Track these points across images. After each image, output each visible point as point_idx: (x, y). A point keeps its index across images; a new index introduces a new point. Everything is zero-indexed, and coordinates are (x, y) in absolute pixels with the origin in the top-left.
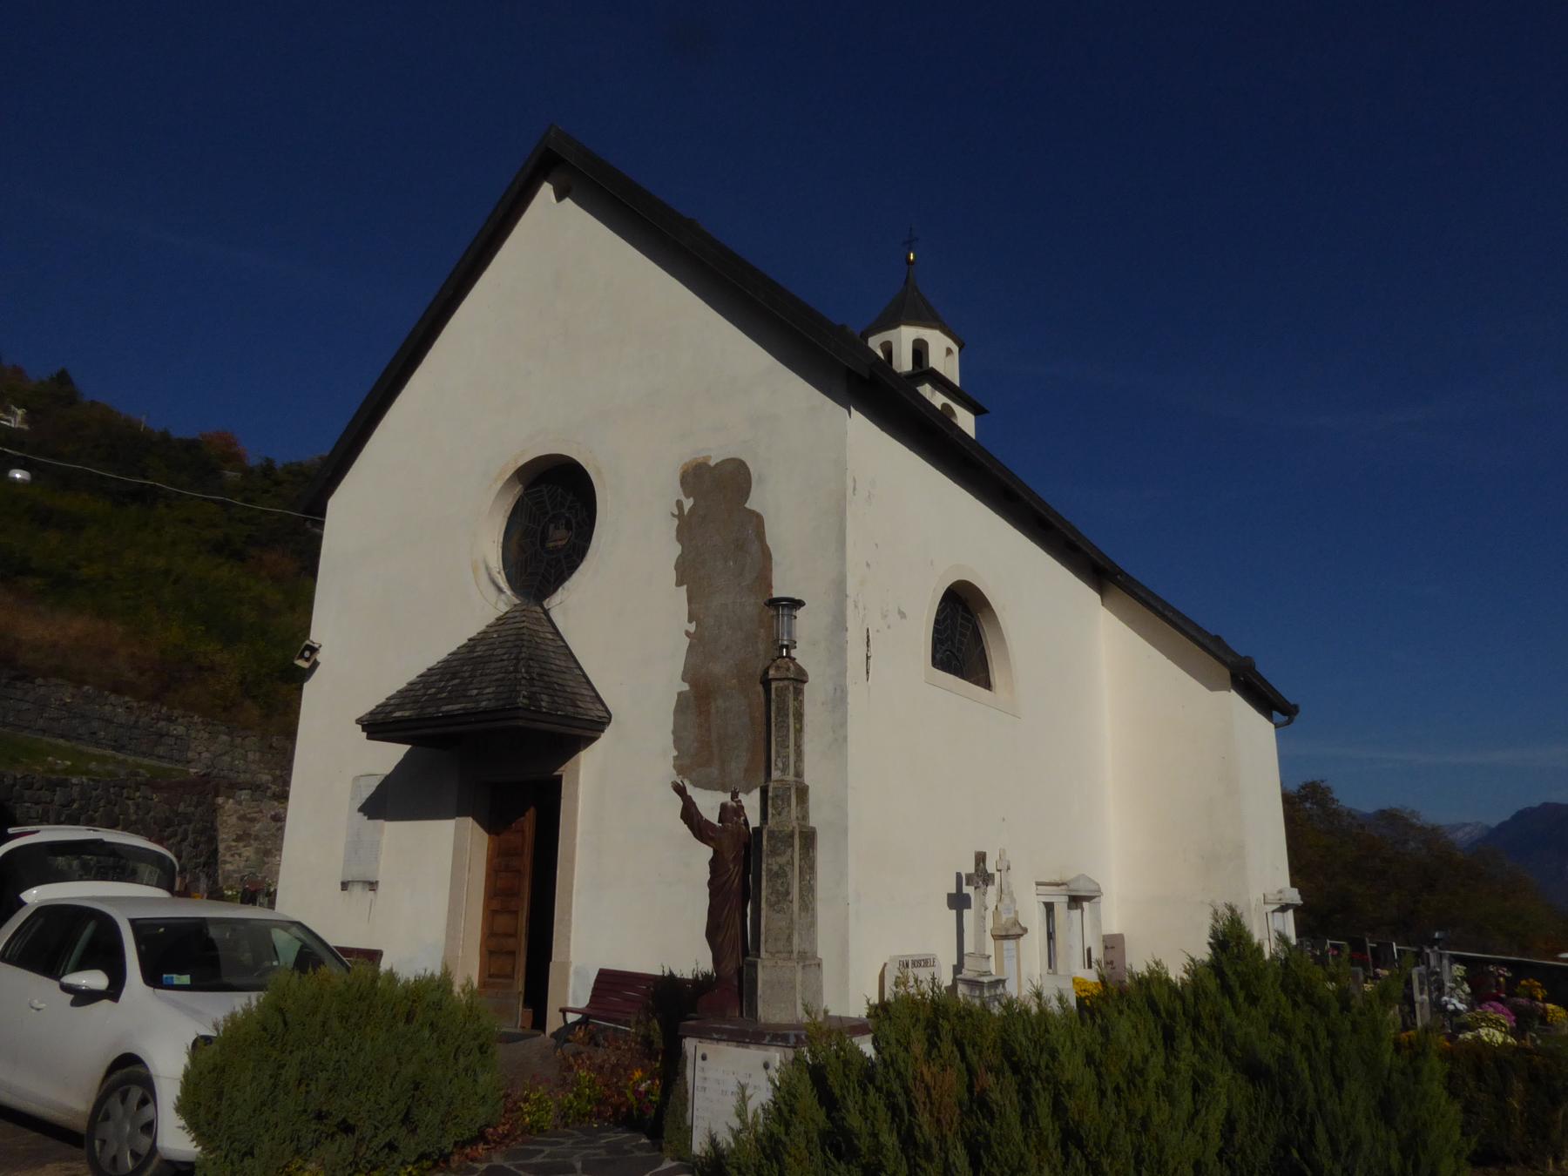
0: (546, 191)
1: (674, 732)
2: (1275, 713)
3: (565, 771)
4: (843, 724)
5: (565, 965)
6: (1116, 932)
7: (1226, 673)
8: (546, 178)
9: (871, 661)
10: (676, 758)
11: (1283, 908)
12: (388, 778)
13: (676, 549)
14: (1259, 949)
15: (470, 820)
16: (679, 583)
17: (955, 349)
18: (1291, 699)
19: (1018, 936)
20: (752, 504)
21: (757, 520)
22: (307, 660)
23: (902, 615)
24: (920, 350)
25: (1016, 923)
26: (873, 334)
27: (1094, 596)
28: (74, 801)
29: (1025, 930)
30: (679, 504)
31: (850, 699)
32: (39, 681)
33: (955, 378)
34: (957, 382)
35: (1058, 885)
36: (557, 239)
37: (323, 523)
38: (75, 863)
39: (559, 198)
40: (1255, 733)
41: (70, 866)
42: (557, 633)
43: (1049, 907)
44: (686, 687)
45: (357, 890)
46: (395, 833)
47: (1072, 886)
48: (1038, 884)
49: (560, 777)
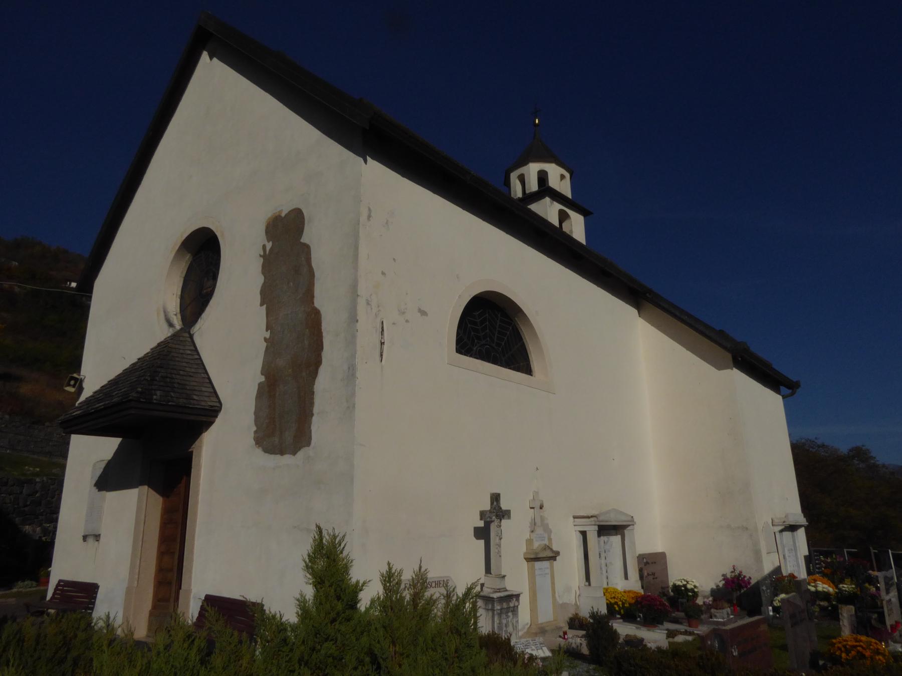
0: (205, 56)
1: (255, 413)
2: (782, 388)
3: (194, 448)
4: (353, 394)
5: (189, 591)
6: (660, 550)
7: (729, 356)
8: (204, 49)
9: (385, 347)
10: (256, 432)
11: (792, 528)
12: (109, 462)
13: (261, 280)
14: (357, 589)
15: (146, 487)
16: (262, 305)
17: (567, 175)
18: (794, 378)
19: (553, 558)
20: (305, 239)
21: (307, 248)
22: (74, 386)
23: (423, 313)
24: (543, 177)
25: (548, 548)
26: (512, 171)
27: (632, 311)
28: (37, 492)
29: (558, 553)
30: (264, 247)
31: (358, 374)
32: (47, 424)
33: (568, 193)
34: (570, 196)
35: (588, 517)
36: (217, 91)
37: (91, 297)
38: (38, 529)
39: (211, 58)
40: (768, 405)
41: (34, 531)
42: (196, 350)
43: (584, 533)
44: (263, 379)
45: (91, 540)
46: (112, 497)
47: (601, 518)
48: (575, 517)
49: (192, 452)
